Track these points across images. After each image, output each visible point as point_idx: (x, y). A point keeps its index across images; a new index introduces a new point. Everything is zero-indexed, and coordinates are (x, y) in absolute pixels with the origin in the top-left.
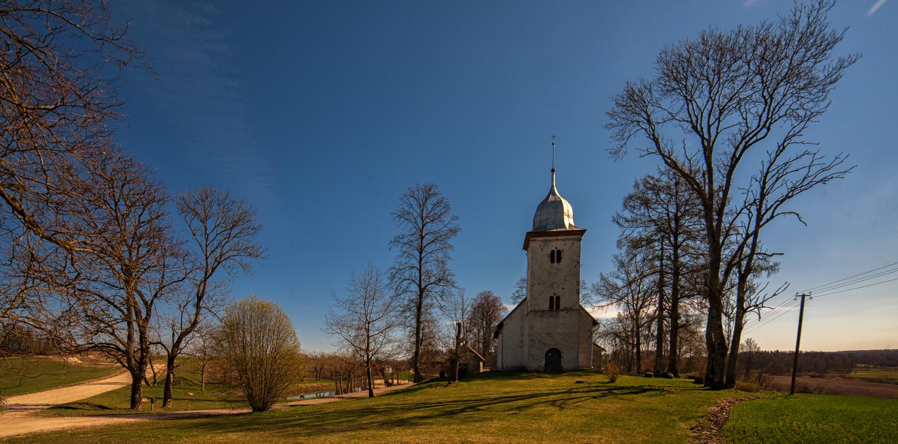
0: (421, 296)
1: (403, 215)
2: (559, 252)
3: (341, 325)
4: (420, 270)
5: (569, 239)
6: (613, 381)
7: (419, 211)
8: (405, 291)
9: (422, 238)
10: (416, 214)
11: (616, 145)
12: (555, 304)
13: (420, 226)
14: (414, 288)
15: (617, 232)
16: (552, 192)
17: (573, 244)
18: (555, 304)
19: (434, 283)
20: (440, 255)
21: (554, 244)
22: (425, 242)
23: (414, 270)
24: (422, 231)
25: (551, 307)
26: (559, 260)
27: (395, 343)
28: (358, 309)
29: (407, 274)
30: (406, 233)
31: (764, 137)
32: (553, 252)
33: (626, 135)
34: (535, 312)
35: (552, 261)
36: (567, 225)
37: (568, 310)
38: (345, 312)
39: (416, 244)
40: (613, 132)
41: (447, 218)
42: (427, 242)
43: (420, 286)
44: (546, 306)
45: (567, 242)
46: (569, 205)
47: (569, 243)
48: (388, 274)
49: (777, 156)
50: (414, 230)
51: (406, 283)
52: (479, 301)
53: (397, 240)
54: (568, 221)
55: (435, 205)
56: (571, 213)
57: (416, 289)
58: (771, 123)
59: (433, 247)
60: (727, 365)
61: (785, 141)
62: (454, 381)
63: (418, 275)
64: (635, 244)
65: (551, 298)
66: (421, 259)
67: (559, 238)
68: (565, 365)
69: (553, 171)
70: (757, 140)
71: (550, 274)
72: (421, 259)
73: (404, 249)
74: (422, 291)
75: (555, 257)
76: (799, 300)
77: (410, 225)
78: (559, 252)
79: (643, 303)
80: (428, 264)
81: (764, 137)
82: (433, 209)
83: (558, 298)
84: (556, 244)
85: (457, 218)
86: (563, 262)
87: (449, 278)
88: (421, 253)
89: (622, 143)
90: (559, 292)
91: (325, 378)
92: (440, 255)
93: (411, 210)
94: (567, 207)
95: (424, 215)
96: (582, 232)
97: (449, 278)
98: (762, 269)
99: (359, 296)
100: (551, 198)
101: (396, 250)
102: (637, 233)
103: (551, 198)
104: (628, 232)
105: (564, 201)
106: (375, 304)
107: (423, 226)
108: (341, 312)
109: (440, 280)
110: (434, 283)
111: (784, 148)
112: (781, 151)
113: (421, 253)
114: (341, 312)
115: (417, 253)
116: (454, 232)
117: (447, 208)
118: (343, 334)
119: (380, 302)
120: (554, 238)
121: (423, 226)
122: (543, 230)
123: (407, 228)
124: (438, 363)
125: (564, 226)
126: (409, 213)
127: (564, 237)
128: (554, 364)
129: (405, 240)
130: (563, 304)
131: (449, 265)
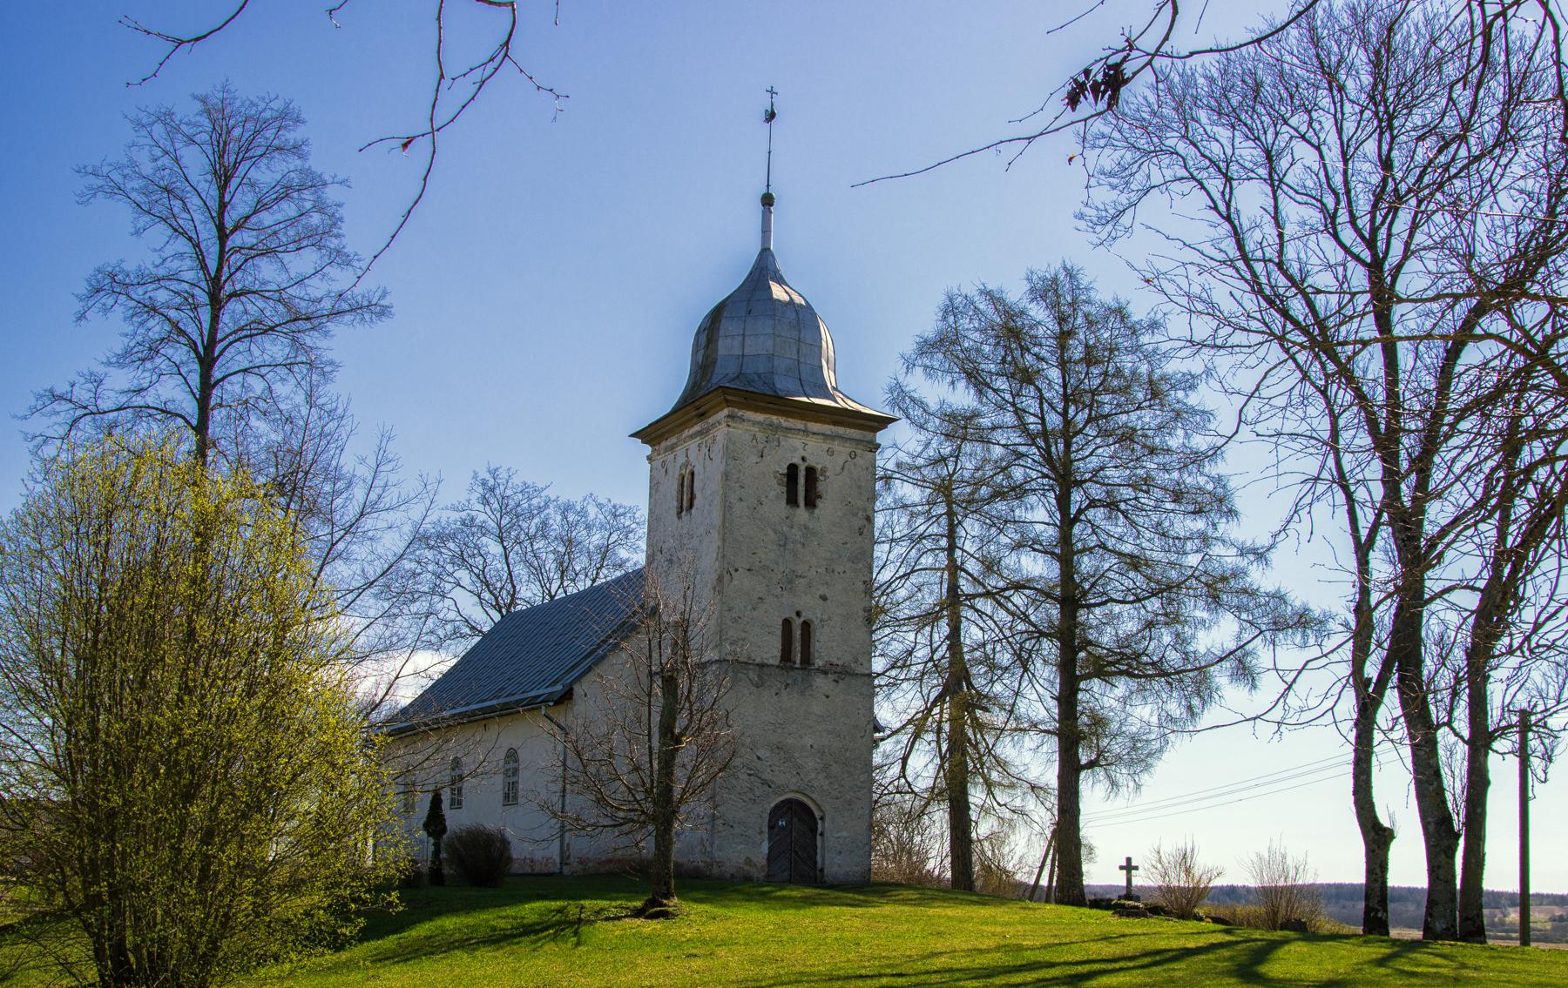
4: (201, 428)
9: (217, 304)
11: (1104, 196)
17: (853, 455)
21: (796, 442)
25: (786, 655)
32: (793, 469)
35: (792, 500)
44: (770, 651)
47: (842, 450)
60: (1261, 978)
65: (787, 623)
66: (207, 386)
70: (492, 59)
71: (783, 543)
72: (207, 386)
75: (801, 485)
79: (1422, 485)
84: (806, 446)
86: (825, 507)
90: (812, 609)
101: (113, 329)
116: (372, 309)
120: (799, 424)
124: (711, 662)
127: (827, 429)
130: (826, 648)
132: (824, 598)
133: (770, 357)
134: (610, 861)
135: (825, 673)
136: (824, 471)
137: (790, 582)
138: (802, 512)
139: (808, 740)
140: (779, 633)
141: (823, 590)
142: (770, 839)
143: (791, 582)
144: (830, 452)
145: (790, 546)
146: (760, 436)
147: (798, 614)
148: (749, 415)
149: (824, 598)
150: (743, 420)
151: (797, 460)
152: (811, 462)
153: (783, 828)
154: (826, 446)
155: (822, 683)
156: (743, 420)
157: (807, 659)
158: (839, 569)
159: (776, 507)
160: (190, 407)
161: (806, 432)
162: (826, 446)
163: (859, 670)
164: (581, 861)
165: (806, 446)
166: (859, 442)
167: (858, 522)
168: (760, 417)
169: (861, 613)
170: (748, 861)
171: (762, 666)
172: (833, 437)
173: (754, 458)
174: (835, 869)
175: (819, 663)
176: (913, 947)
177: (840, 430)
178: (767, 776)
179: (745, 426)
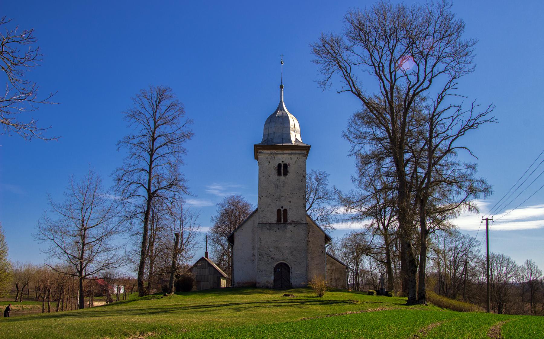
0: (149, 201)
1: (134, 116)
2: (286, 166)
3: (54, 230)
4: (150, 173)
5: (295, 154)
6: (320, 296)
7: (152, 113)
8: (132, 195)
9: (154, 140)
10: (148, 116)
11: (322, 77)
12: (282, 216)
13: (153, 127)
14: (142, 192)
15: (347, 146)
16: (280, 107)
17: (298, 158)
18: (282, 216)
19: (165, 188)
20: (172, 159)
21: (280, 157)
22: (157, 144)
23: (144, 173)
24: (154, 134)
25: (279, 220)
26: (286, 173)
27: (119, 255)
28: (75, 214)
29: (135, 177)
30: (137, 134)
31: (427, 88)
32: (279, 165)
33: (331, 71)
34: (262, 224)
35: (279, 174)
36: (293, 140)
37: (296, 224)
38: (61, 217)
39: (147, 145)
40: (319, 66)
41: (182, 120)
42: (159, 145)
43: (149, 190)
44: (273, 219)
45: (293, 156)
46: (296, 121)
47: (295, 158)
48: (114, 176)
49: (439, 103)
50: (145, 132)
51: (133, 186)
52: (226, 207)
53: (127, 141)
54: (295, 137)
55: (169, 108)
56: (298, 128)
57: (146, 194)
58: (432, 78)
59: (165, 149)
61: (443, 92)
62: (170, 293)
63: (147, 178)
64: (365, 160)
65: (279, 211)
66: (151, 162)
67: (285, 152)
68: (294, 281)
69: (281, 87)
71: (277, 187)
72: (151, 162)
73: (134, 150)
74: (151, 196)
75: (282, 169)
76: (485, 221)
77: (141, 127)
78: (286, 166)
80: (160, 168)
81: (427, 88)
82: (166, 111)
83: (285, 211)
84: (283, 158)
85: (191, 122)
86: (290, 175)
87: (181, 183)
88: (151, 155)
89: (327, 77)
91: (28, 299)
92: (172, 159)
93: (143, 111)
94: (294, 122)
95: (157, 117)
96: (309, 147)
97: (181, 183)
98: (479, 190)
99: (76, 201)
100: (279, 113)
102: (368, 149)
103: (279, 113)
104: (357, 148)
105: (291, 116)
106: (94, 210)
107: (155, 128)
108: (55, 217)
109: (171, 185)
110: (165, 188)
111: (442, 98)
112: (441, 100)
113: (151, 155)
114: (55, 217)
115: (147, 156)
116: (188, 136)
117: (181, 111)
118: (56, 240)
119: (99, 208)
120: (281, 152)
121: (155, 128)
122: (270, 143)
123: (138, 129)
125: (291, 142)
126: (141, 113)
127: (290, 152)
128: (282, 279)
129: (135, 141)
130: (292, 216)
131: (182, 169)
132: (290, 202)
133: (274, 133)
134: (246, 283)
135: (291, 224)
136: (289, 164)
137: (279, 198)
138: (282, 178)
139: (286, 245)
140: (276, 213)
141: (290, 200)
142: (274, 275)
143: (279, 198)
144: (291, 158)
145: (279, 188)
146: (269, 157)
147: (282, 207)
148: (265, 151)
149: (290, 202)
150: (263, 153)
151: (280, 162)
152: (285, 162)
153: (279, 271)
154: (289, 157)
155: (290, 227)
156: (263, 153)
157: (286, 220)
158: (294, 193)
159: (274, 176)
160: (148, 169)
161: (283, 154)
162: (289, 157)
163: (302, 222)
164: (238, 283)
165: (283, 158)
166: (299, 154)
167: (301, 178)
168: (269, 151)
169: (302, 205)
170: (267, 282)
171: (271, 224)
172: (291, 154)
173: (268, 164)
174: (295, 283)
175: (289, 221)
176: (194, 316)
177: (294, 151)
178: (273, 256)
179: (264, 155)
